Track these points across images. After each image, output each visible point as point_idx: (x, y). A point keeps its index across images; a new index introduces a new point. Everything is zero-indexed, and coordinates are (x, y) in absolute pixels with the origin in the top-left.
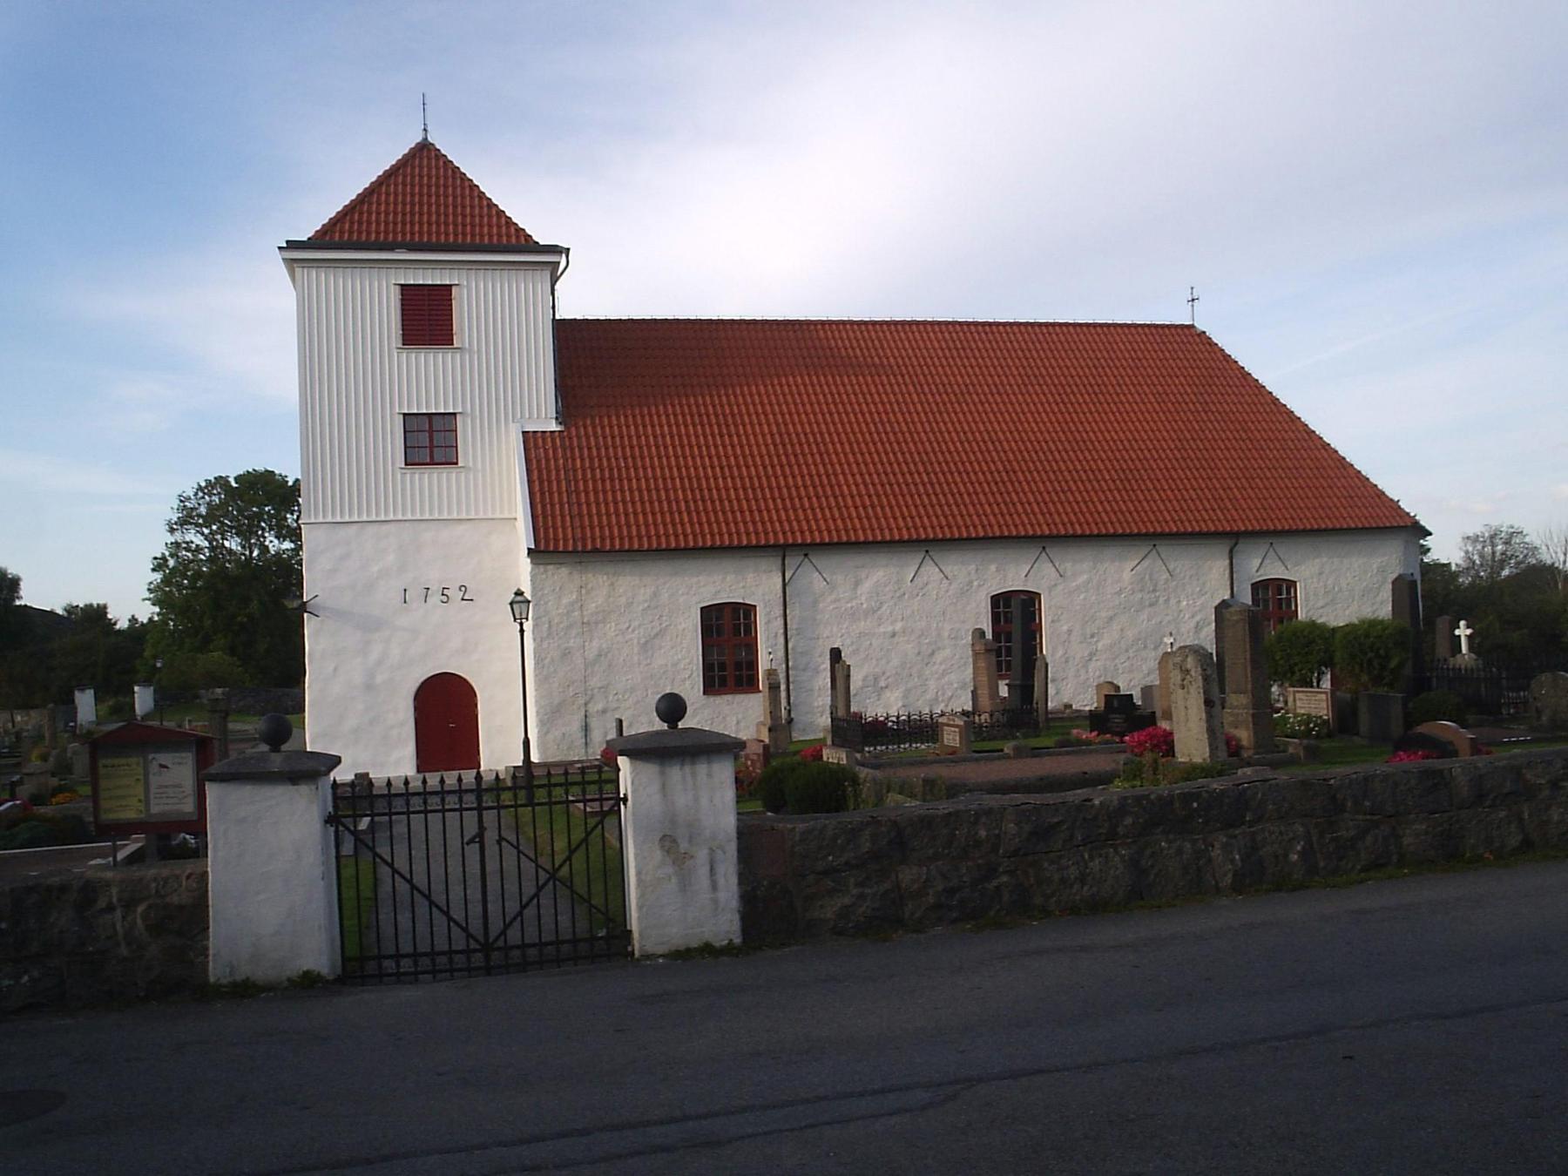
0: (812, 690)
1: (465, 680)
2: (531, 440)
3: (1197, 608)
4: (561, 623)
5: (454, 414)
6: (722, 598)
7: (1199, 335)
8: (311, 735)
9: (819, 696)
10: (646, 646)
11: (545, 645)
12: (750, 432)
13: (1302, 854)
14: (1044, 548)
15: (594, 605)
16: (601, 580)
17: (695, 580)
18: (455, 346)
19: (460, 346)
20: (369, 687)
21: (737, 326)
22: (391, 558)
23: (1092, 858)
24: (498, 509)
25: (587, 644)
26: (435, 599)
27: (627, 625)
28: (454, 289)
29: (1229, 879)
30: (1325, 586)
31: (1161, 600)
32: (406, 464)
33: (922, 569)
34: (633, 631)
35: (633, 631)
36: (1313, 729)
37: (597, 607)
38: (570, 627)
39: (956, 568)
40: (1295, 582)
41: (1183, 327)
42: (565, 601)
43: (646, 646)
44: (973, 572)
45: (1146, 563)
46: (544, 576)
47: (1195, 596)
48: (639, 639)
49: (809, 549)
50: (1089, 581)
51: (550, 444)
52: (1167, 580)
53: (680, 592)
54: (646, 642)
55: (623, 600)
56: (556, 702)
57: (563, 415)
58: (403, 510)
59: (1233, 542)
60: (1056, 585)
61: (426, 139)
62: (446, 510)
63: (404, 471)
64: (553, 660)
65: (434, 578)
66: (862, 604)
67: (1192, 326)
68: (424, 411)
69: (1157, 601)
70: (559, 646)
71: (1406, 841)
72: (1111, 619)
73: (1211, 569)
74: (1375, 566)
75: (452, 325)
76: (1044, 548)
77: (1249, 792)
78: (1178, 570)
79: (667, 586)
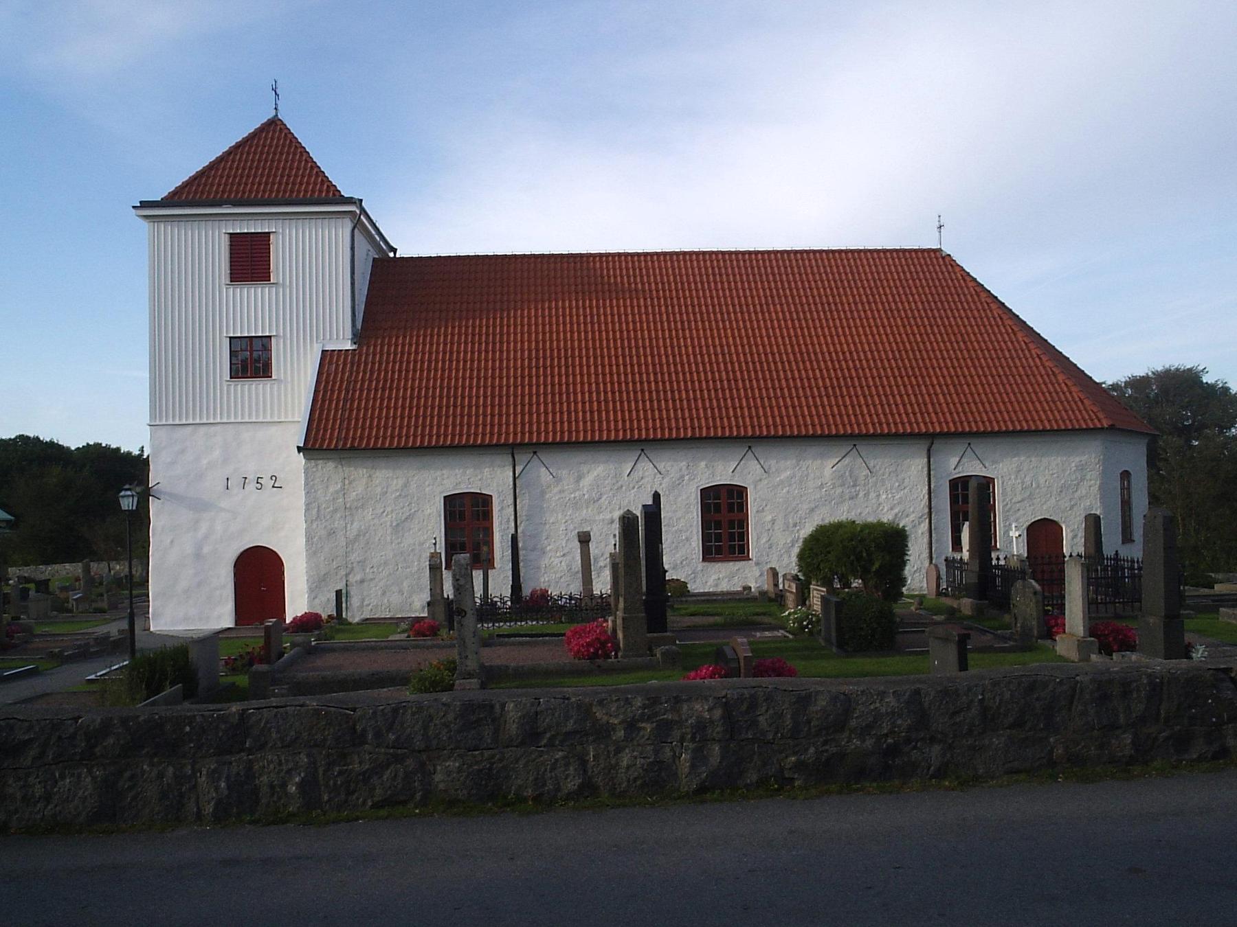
0: (539, 568)
1: (275, 552)
2: (327, 357)
3: (896, 502)
4: (328, 508)
5: (270, 337)
6: (461, 489)
7: (943, 258)
8: (152, 594)
9: (546, 573)
10: (398, 528)
11: (314, 526)
12: (778, 334)
13: (300, 786)
14: (750, 447)
15: (354, 493)
16: (361, 472)
17: (439, 473)
18: (272, 281)
19: (275, 282)
20: (198, 556)
21: (526, 260)
22: (217, 453)
23: (63, 777)
24: (290, 413)
25: (349, 525)
26: (251, 486)
27: (382, 510)
28: (272, 236)
29: (209, 809)
30: (1023, 483)
31: (861, 494)
32: (231, 378)
33: (638, 465)
34: (387, 515)
35: (387, 515)
36: (807, 627)
37: (357, 495)
38: (335, 511)
39: (669, 464)
40: (994, 479)
41: (929, 251)
42: (331, 490)
43: (398, 528)
44: (684, 468)
45: (847, 461)
46: (314, 469)
47: (894, 491)
48: (392, 522)
49: (536, 447)
50: (793, 476)
51: (342, 360)
52: (867, 476)
53: (427, 483)
54: (398, 524)
55: (379, 490)
56: (323, 573)
57: (357, 337)
58: (235, 415)
59: (930, 441)
60: (760, 480)
61: (277, 115)
62: (233, 415)
63: (228, 383)
64: (320, 538)
65: (251, 470)
66: (584, 495)
67: (940, 250)
68: (246, 335)
69: (857, 495)
70: (325, 527)
71: (438, 777)
72: (812, 510)
73: (909, 467)
74: (1073, 465)
75: (269, 265)
76: (750, 447)
77: (254, 718)
78: (878, 467)
79: (416, 478)
